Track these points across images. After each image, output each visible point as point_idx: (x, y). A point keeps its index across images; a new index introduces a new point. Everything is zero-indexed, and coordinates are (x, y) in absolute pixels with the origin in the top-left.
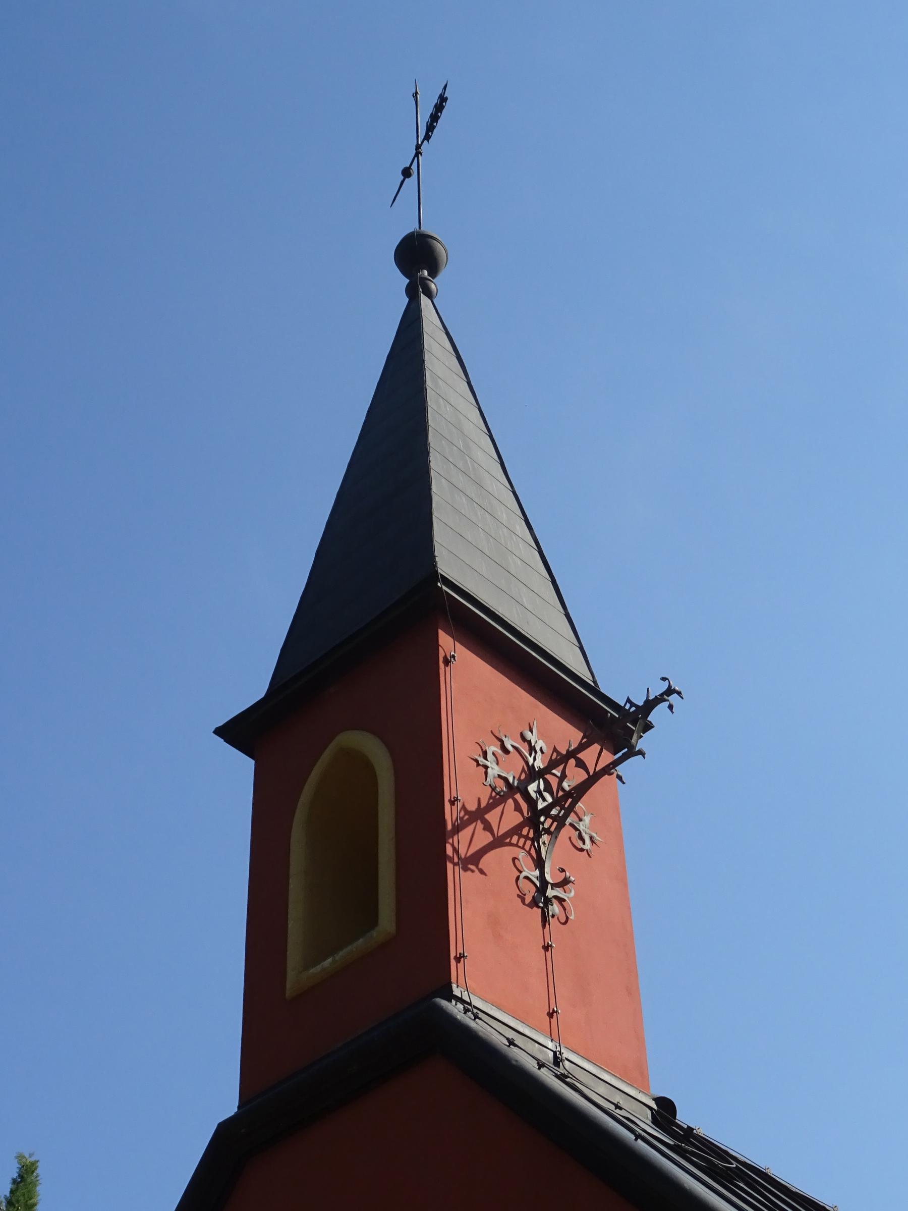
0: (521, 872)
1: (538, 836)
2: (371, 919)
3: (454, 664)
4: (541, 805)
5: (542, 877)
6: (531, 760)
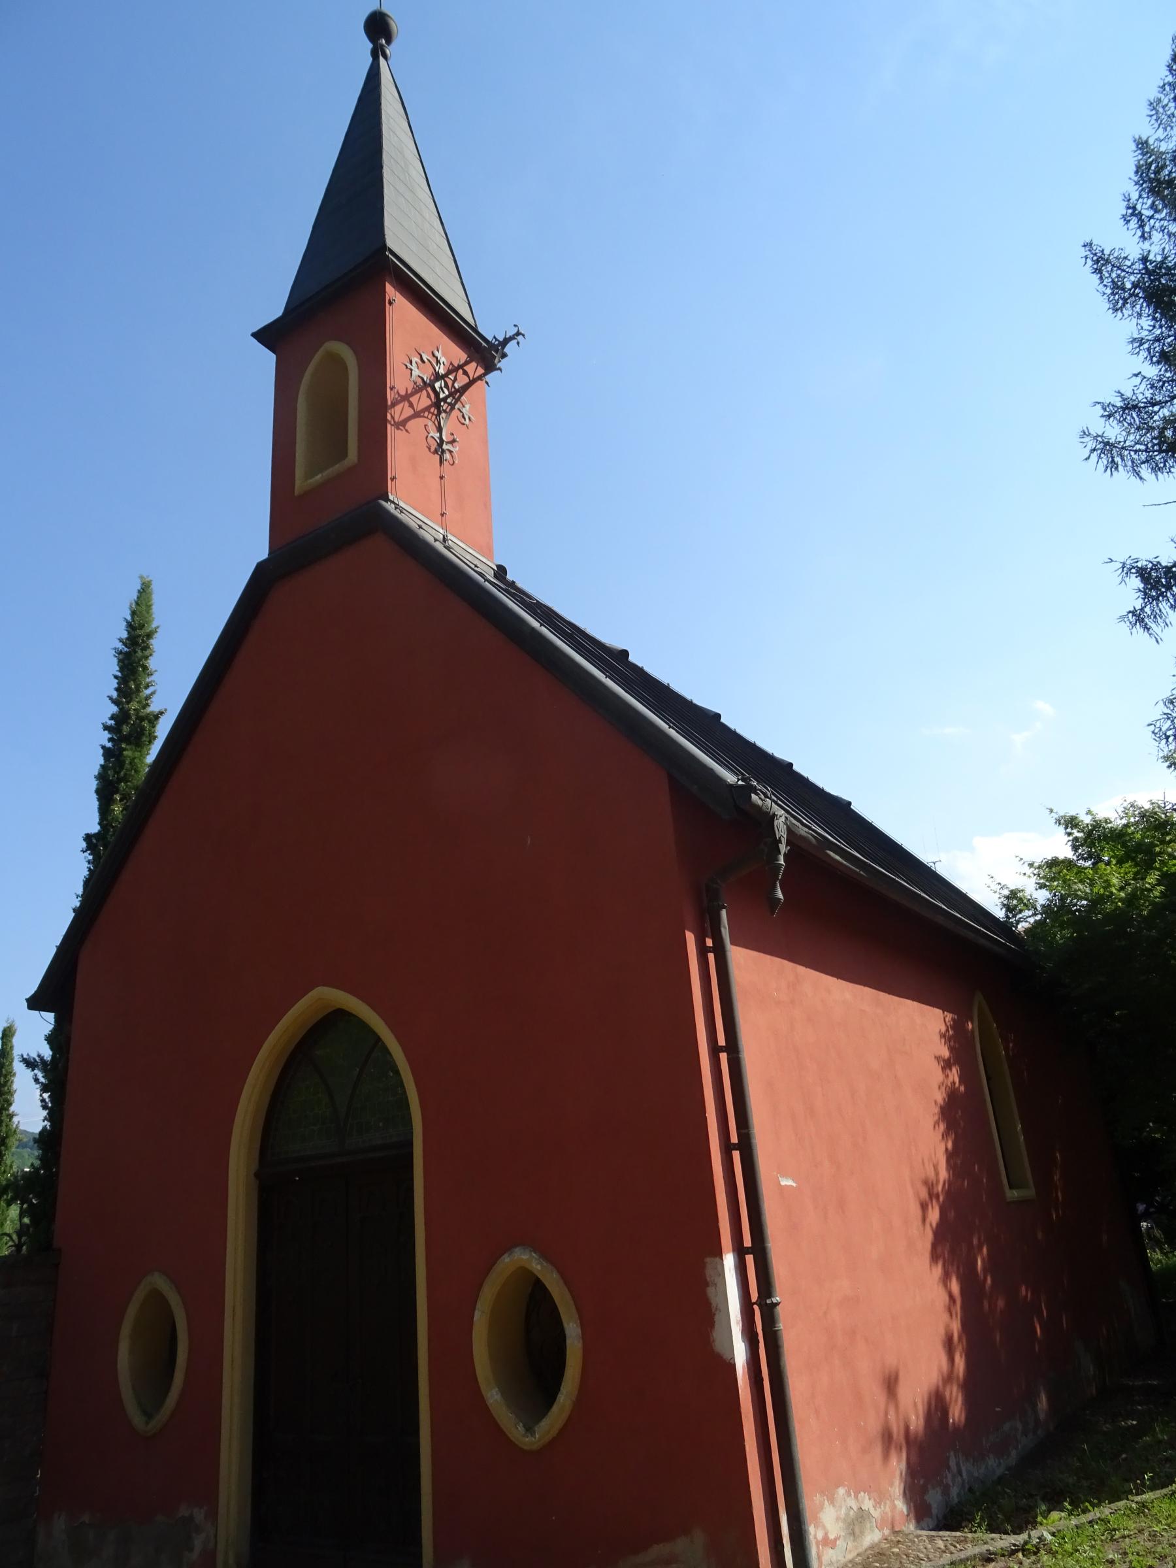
0: (429, 433)
1: (439, 413)
2: (344, 454)
3: (394, 304)
4: (442, 396)
5: (441, 438)
6: (437, 369)
